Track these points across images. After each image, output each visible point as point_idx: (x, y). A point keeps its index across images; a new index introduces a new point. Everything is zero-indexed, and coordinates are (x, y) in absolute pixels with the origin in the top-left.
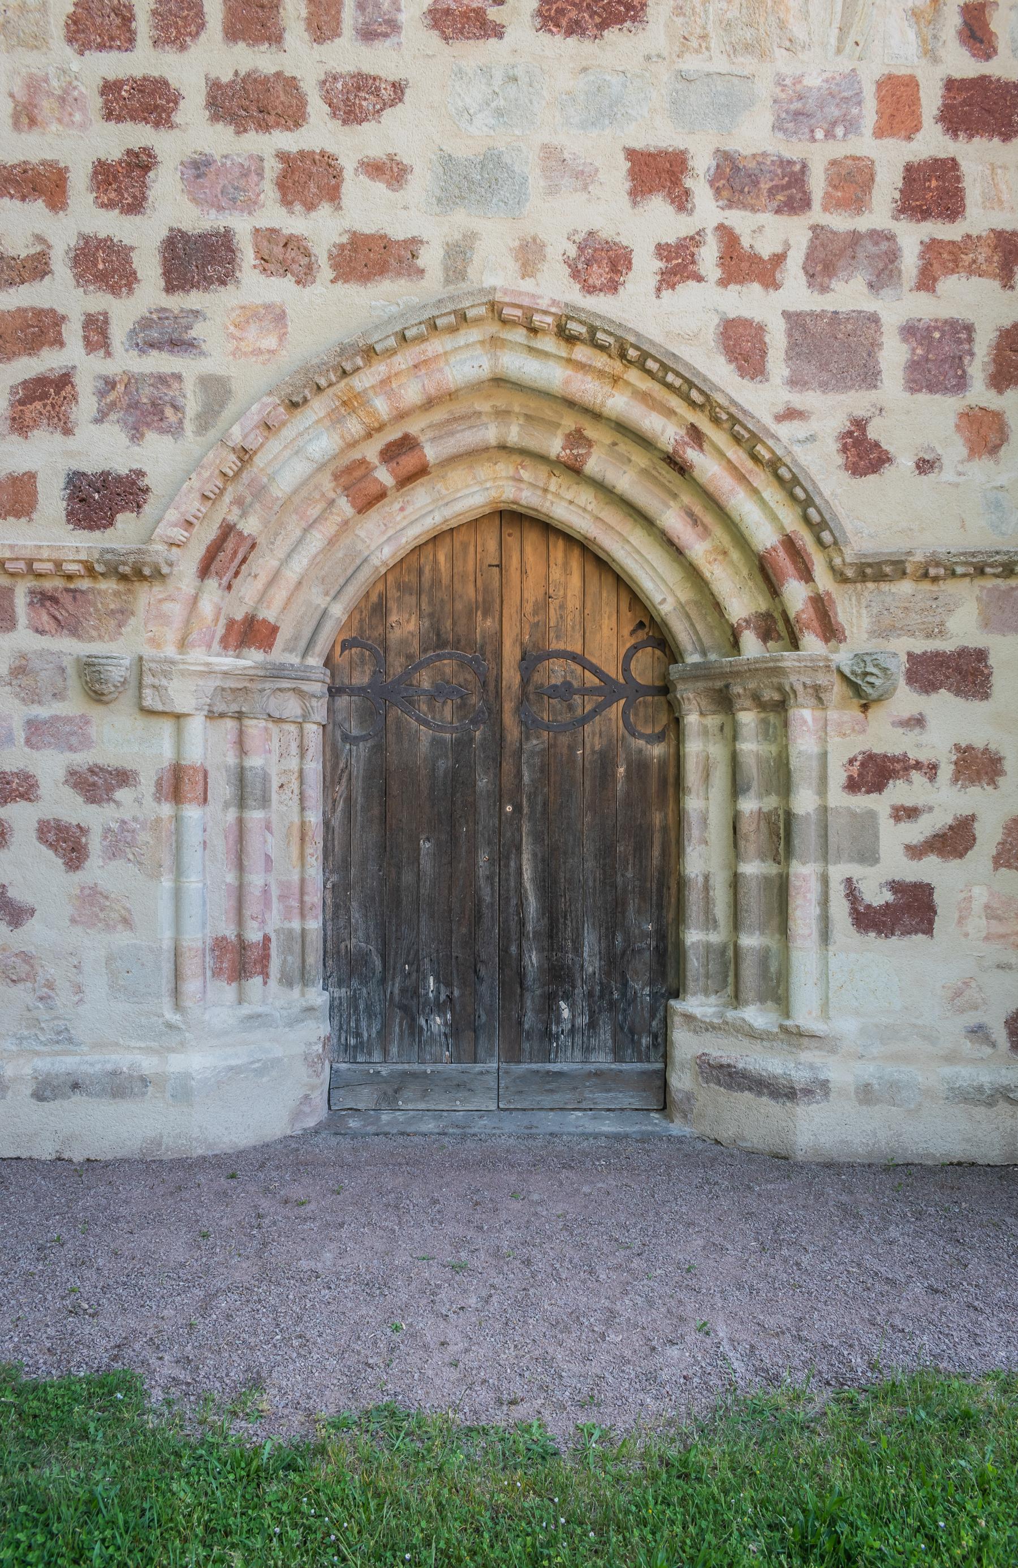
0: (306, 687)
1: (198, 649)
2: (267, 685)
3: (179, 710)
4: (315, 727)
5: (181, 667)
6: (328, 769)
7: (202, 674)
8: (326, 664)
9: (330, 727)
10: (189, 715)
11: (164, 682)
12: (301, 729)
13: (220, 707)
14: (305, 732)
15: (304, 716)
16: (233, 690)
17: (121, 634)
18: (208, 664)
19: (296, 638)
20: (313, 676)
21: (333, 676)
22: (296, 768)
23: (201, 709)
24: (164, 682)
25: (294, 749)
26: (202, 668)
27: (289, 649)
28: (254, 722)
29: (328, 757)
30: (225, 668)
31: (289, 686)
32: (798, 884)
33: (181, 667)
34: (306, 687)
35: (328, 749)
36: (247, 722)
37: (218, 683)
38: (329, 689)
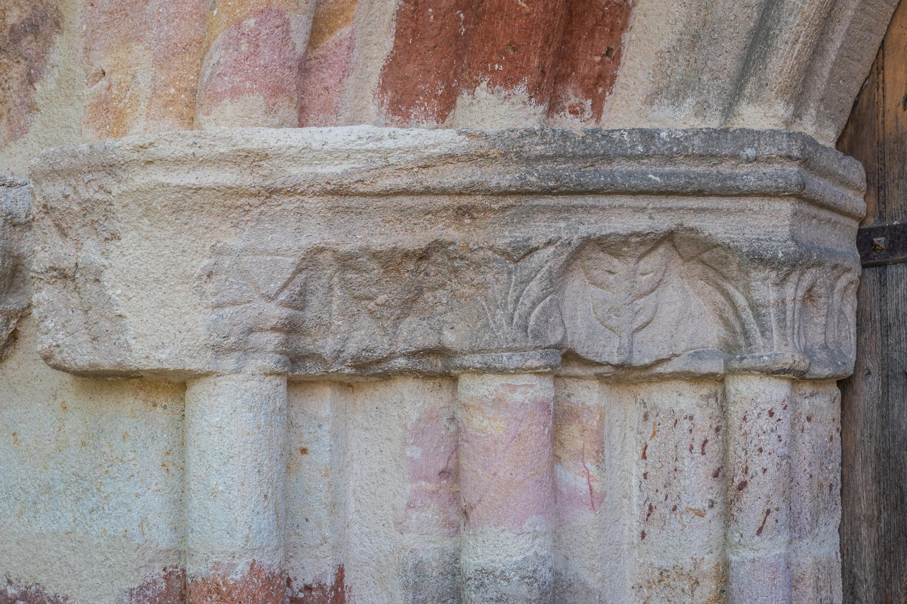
0: (719, 223)
1: (229, 108)
2: (539, 230)
3: (165, 358)
4: (776, 391)
5: (141, 179)
6: (867, 555)
7: (233, 202)
8: (848, 143)
9: (868, 391)
10: (198, 376)
11: (91, 252)
12: (723, 402)
13: (344, 332)
14: (735, 412)
15: (729, 349)
16: (391, 261)
17: (32, 108)
18: (253, 158)
19: (695, 40)
20: (749, 175)
21: (876, 184)
22: (709, 563)
23: (242, 349)
24: (91, 252)
25: (696, 482)
26: (227, 177)
27: (671, 91)
28: (490, 386)
29: (864, 507)
30: (332, 170)
31: (641, 223)
32: (358, 402)
33: (141, 179)
34: (719, 223)
35: (863, 476)
36: (474, 388)
37: (315, 234)
38: (864, 240)
